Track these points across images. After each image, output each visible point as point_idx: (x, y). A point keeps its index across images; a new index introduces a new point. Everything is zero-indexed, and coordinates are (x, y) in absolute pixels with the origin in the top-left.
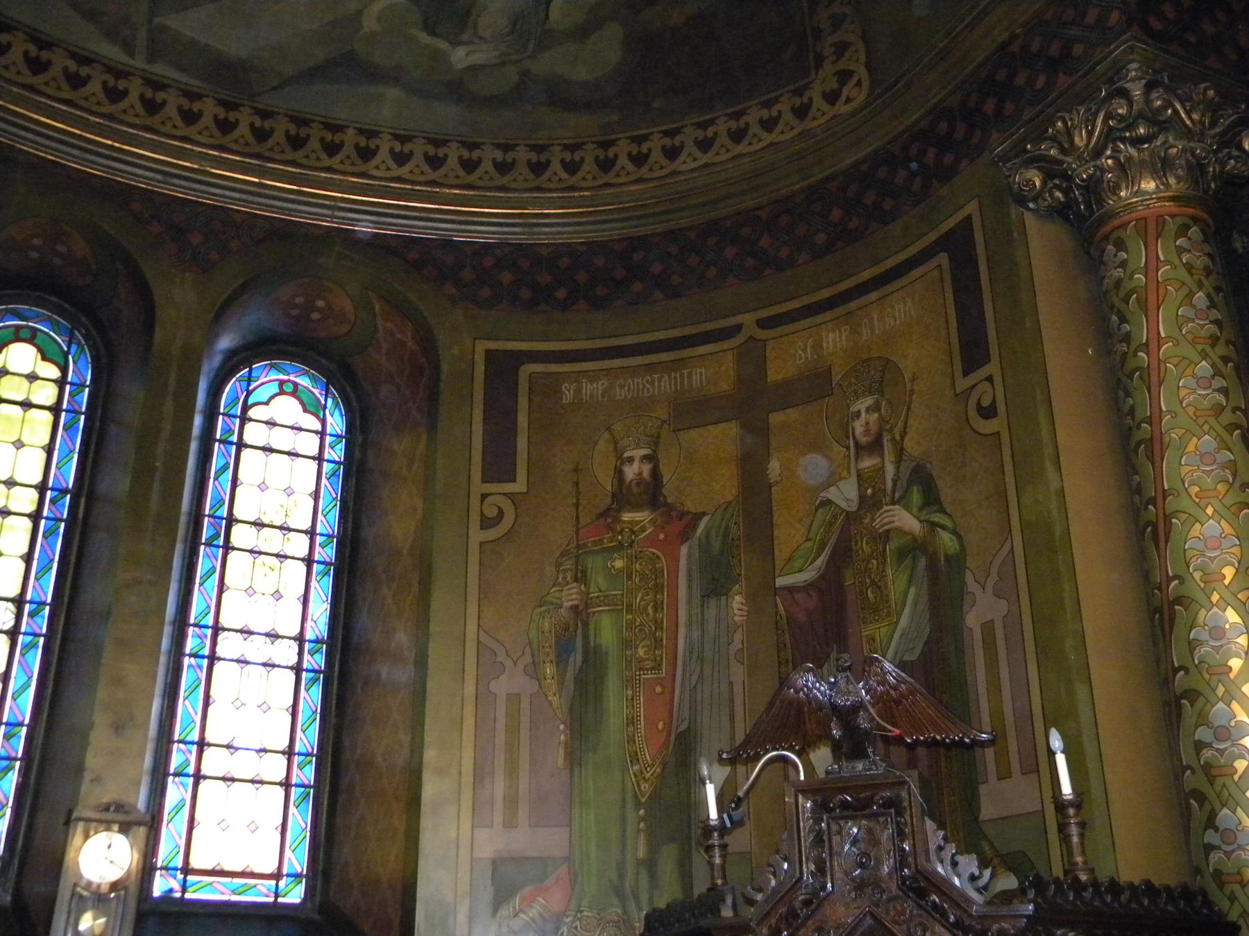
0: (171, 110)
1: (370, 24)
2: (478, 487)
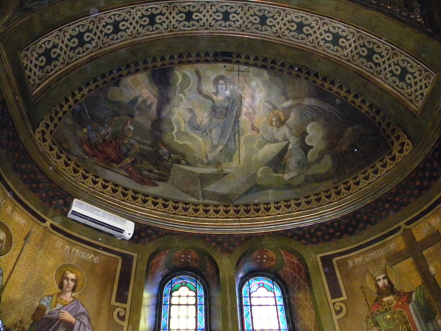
0: (212, 211)
1: (259, 175)
2: (331, 301)
